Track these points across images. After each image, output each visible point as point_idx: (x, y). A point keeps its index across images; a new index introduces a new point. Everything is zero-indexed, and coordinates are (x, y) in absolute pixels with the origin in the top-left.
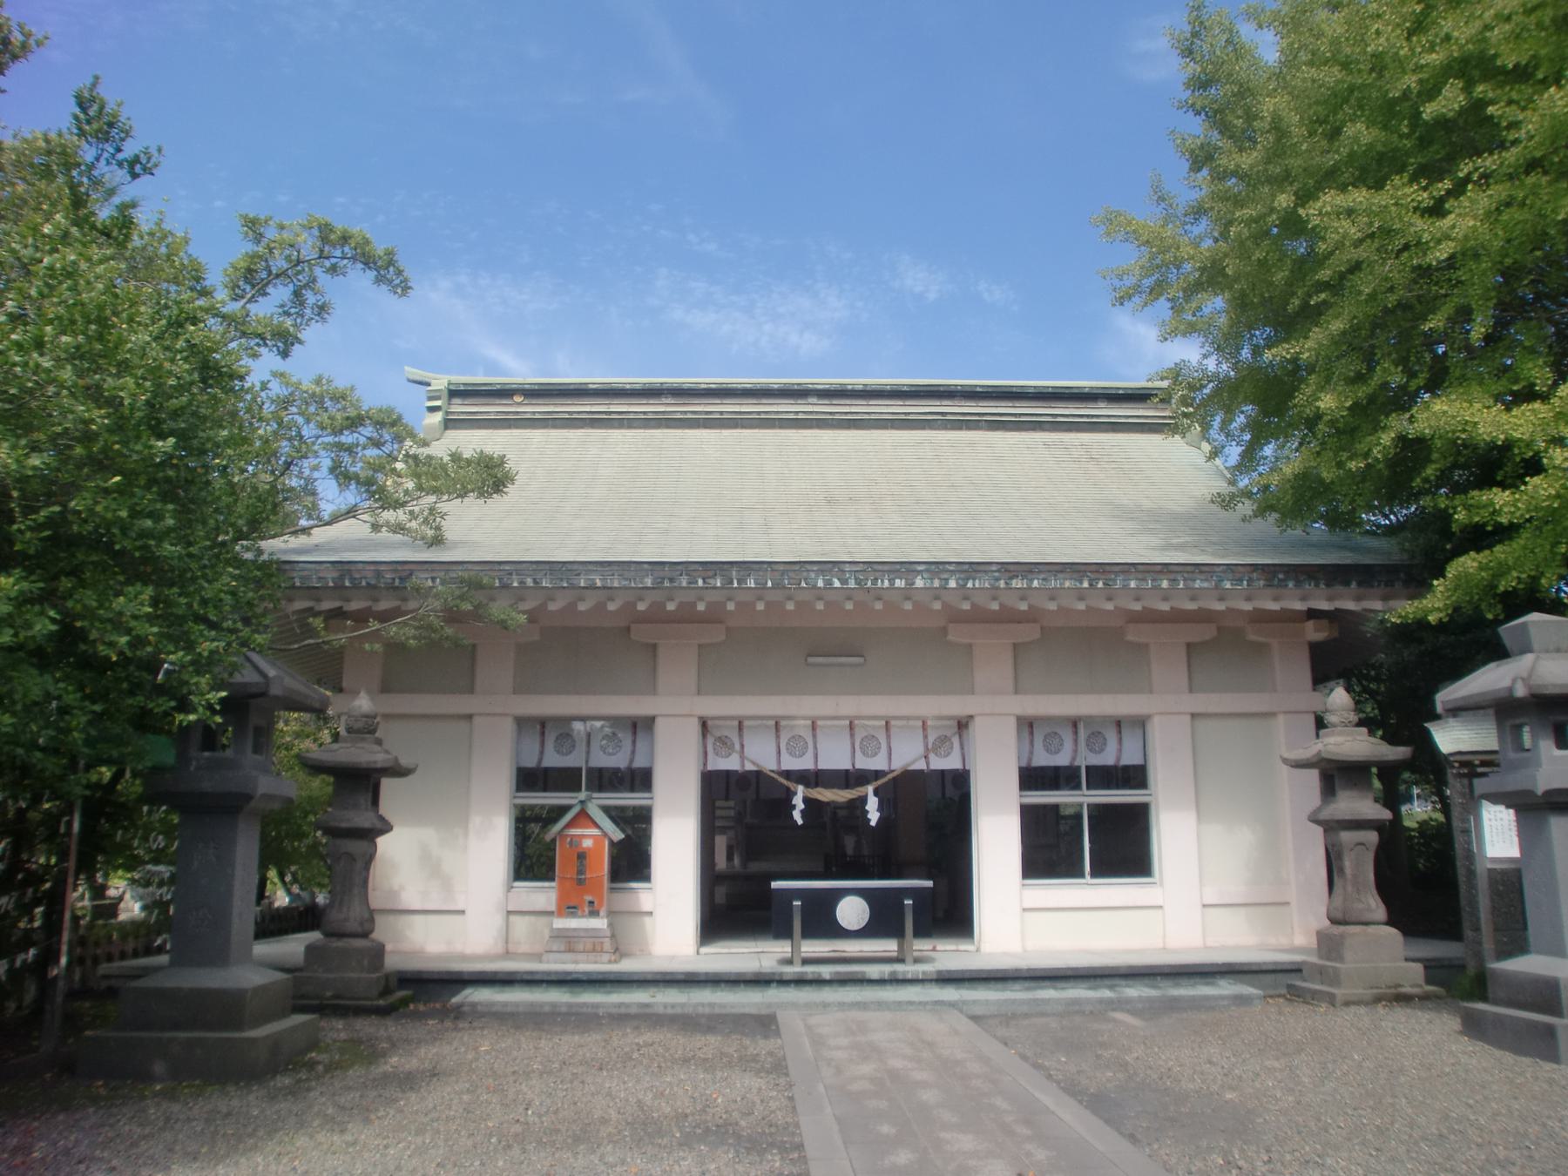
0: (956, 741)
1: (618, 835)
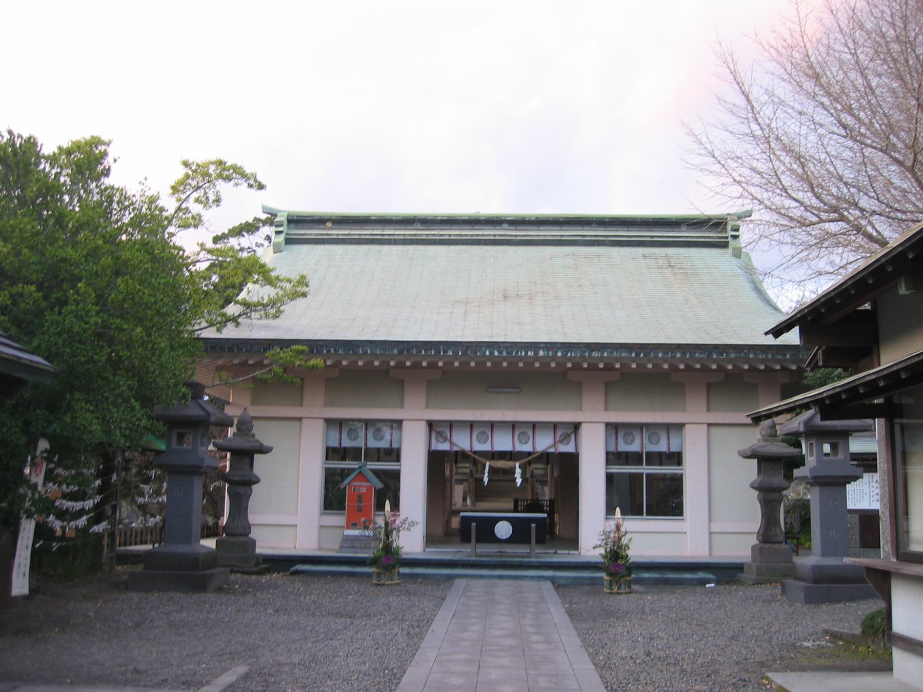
0: (573, 437)
1: (380, 485)
